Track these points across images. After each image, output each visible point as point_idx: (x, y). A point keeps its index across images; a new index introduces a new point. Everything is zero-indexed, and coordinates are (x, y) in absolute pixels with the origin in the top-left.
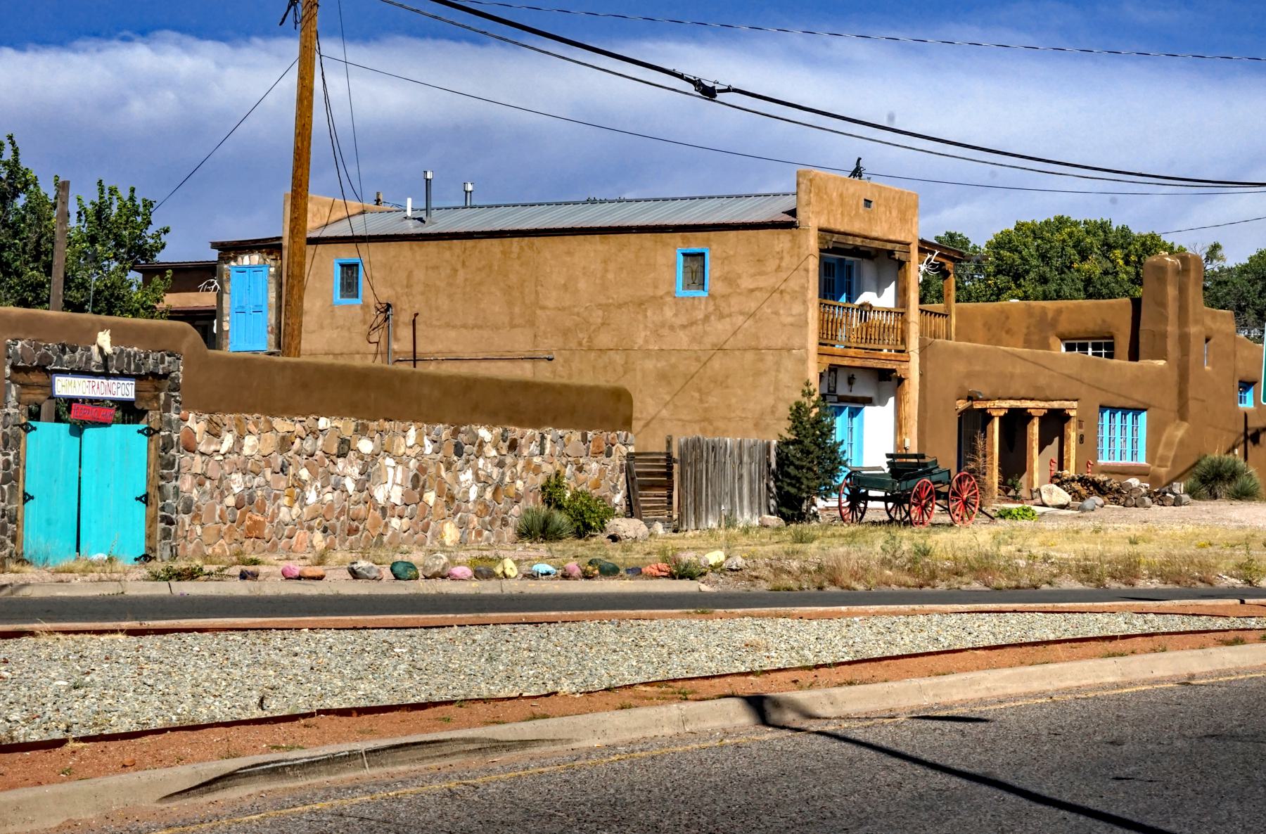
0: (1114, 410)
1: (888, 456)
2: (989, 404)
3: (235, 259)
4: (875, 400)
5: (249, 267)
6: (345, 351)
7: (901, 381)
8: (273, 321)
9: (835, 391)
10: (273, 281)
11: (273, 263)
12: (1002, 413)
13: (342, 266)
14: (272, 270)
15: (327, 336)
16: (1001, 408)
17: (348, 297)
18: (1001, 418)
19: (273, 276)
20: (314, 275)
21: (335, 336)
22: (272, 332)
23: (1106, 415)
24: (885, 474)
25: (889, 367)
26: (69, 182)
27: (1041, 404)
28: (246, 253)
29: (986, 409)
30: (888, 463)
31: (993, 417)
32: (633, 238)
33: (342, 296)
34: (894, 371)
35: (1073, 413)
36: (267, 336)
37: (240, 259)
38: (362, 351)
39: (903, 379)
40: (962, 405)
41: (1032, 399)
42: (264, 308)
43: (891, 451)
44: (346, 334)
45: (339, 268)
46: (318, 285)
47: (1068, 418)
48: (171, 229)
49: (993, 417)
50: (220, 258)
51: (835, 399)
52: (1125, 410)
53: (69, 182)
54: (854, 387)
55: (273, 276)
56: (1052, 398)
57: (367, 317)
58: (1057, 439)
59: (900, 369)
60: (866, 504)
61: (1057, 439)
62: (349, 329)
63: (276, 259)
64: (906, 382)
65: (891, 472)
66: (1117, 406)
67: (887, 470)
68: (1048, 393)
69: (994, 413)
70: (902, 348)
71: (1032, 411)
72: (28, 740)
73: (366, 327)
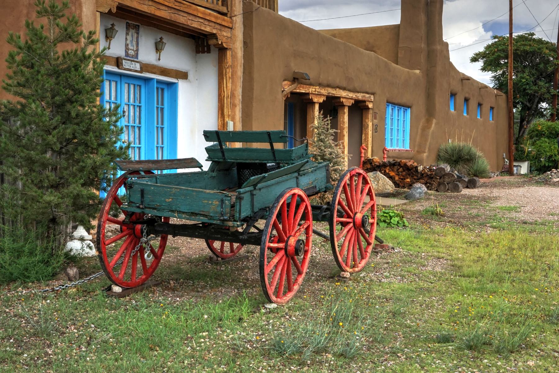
0: (394, 104)
1: (208, 135)
2: (311, 90)
4: (190, 76)
7: (222, 50)
9: (137, 56)
12: (321, 100)
16: (320, 95)
18: (320, 104)
23: (390, 107)
24: (203, 173)
25: (208, 29)
26: (206, 148)
27: (351, 95)
29: (308, 94)
30: (208, 150)
31: (313, 103)
34: (214, 36)
35: (370, 106)
39: (225, 49)
40: (288, 87)
41: (344, 89)
43: (213, 126)
47: (367, 108)
49: (313, 103)
50: (517, 249)
51: (138, 67)
52: (400, 105)
53: (206, 148)
54: (164, 54)
56: (358, 89)
59: (223, 36)
60: (164, 240)
64: (229, 53)
65: (212, 169)
66: (396, 102)
67: (206, 166)
68: (357, 85)
69: (315, 100)
70: (224, 10)
71: (344, 100)
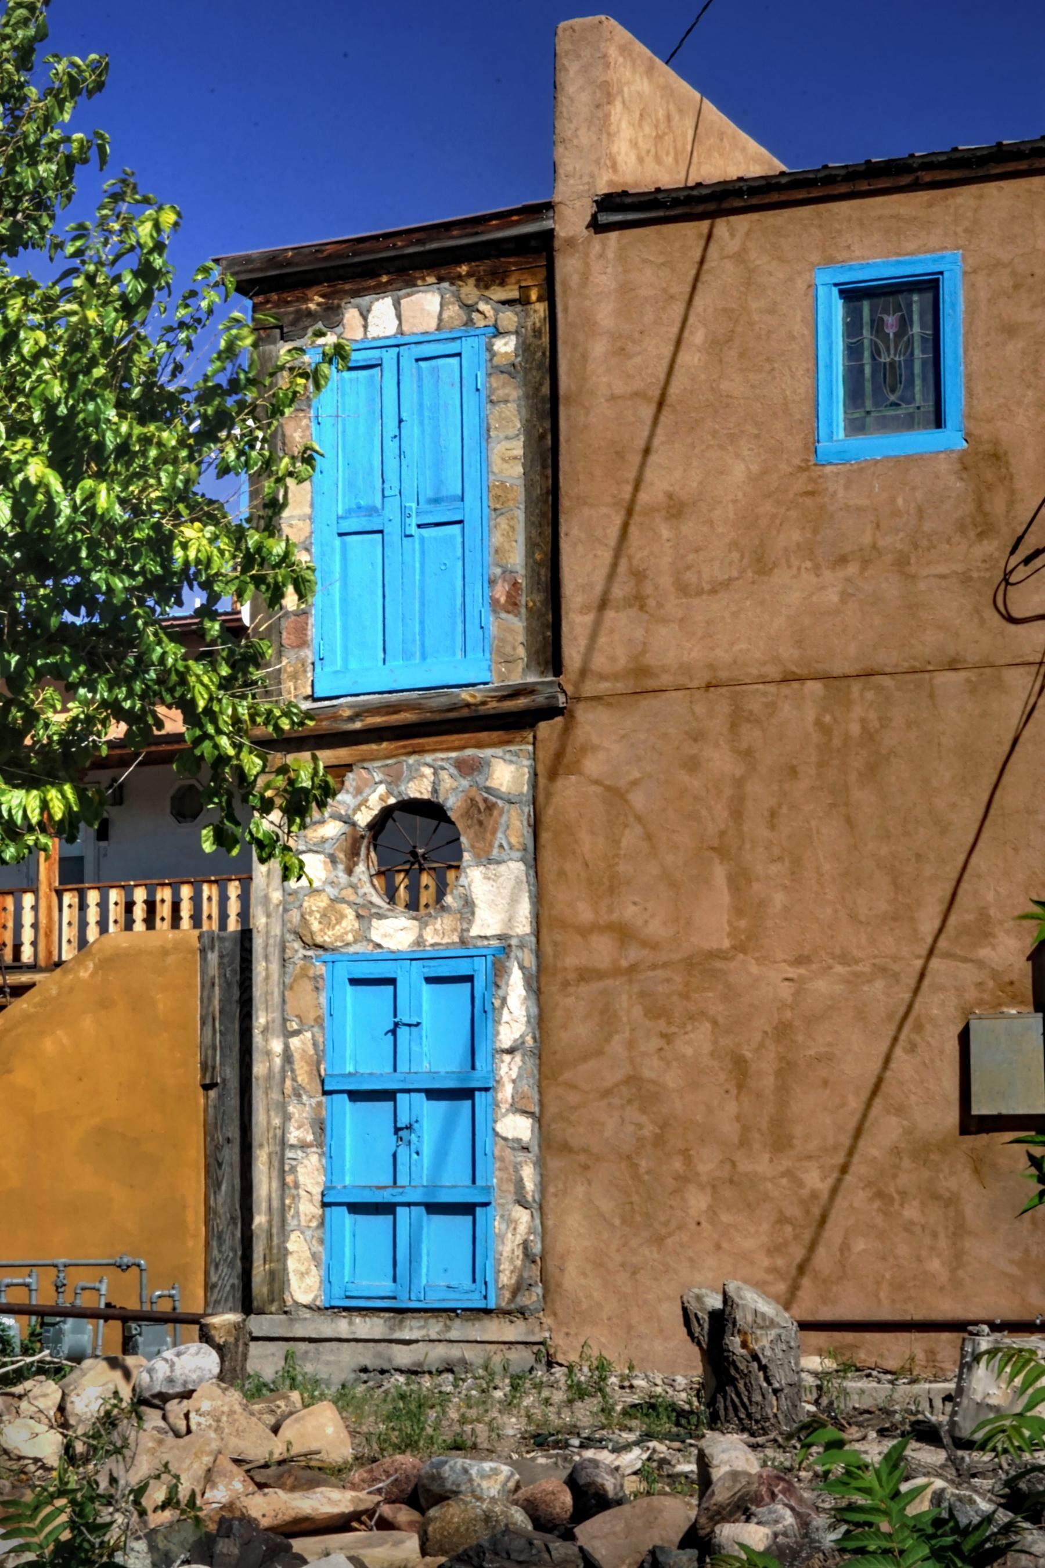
3: (331, 316)
5: (397, 344)
6: (888, 658)
8: (517, 558)
10: (513, 392)
11: (509, 318)
13: (851, 294)
14: (506, 346)
15: (794, 597)
17: (885, 425)
19: (510, 370)
20: (716, 346)
21: (832, 597)
22: (512, 604)
28: (380, 290)
32: (470, 1171)
33: (855, 427)
36: (490, 621)
37: (351, 315)
38: (972, 654)
42: (472, 510)
44: (891, 588)
45: (838, 306)
46: (733, 385)
48: (50, 32)
55: (510, 370)
57: (998, 504)
58: (705, 1346)
61: (705, 1346)
62: (902, 562)
63: (523, 301)
72: (155, 1308)
73: (993, 547)
